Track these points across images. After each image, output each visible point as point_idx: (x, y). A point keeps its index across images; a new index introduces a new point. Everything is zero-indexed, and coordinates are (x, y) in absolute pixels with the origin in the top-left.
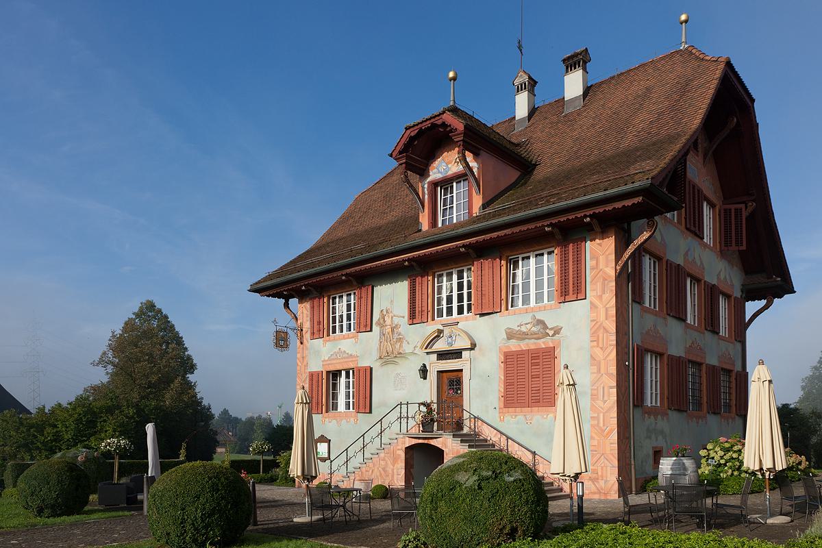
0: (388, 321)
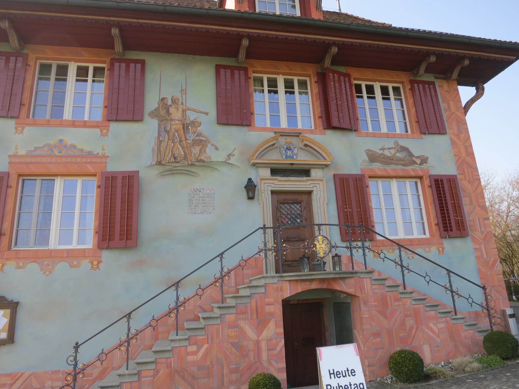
0: (176, 114)
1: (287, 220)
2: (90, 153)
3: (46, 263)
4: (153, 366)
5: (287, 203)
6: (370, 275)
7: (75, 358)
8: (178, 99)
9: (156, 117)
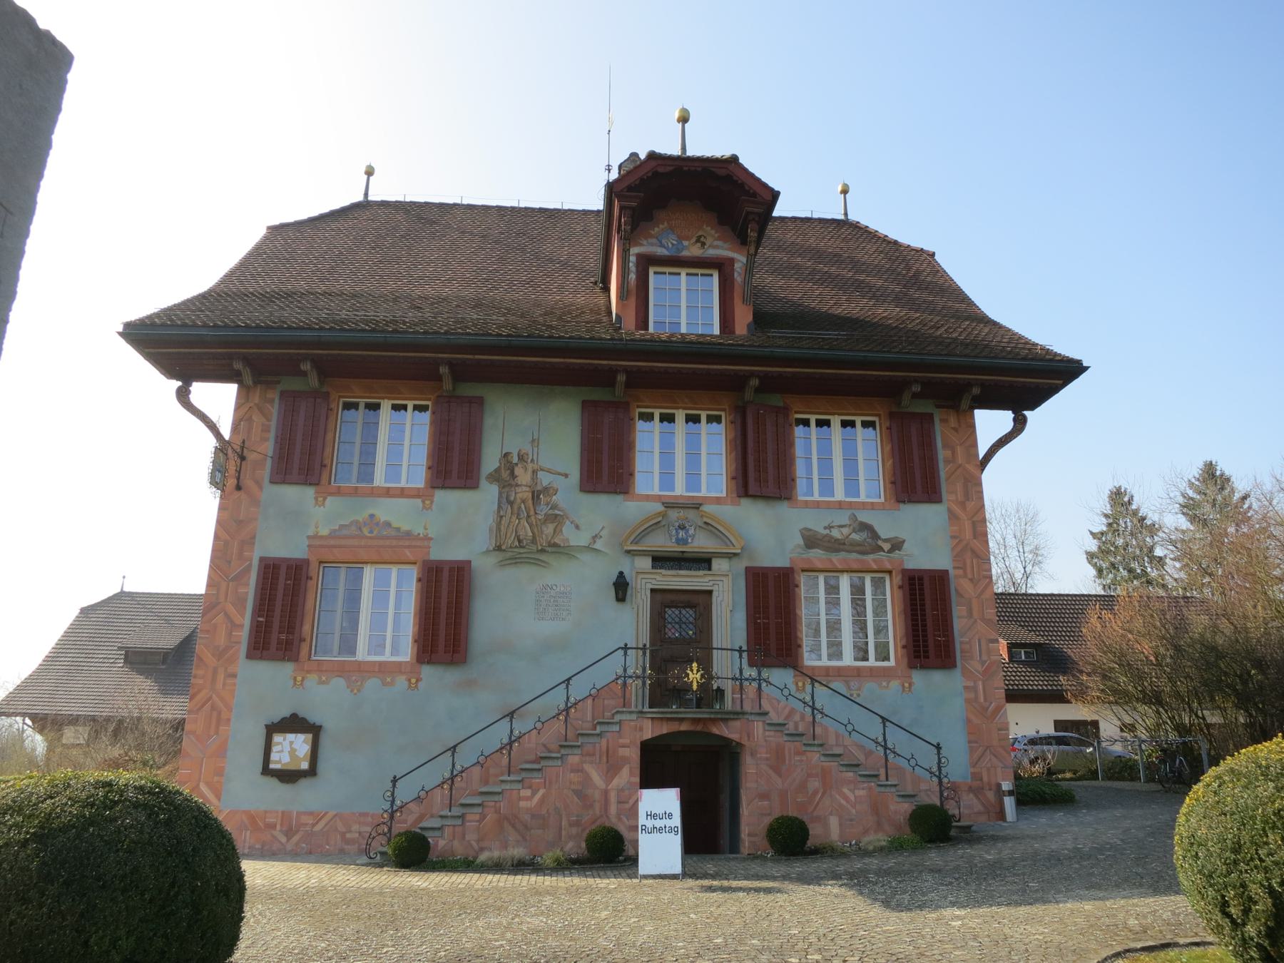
0: (523, 477)
1: (673, 631)
2: (408, 533)
3: (354, 678)
4: (479, 810)
5: (676, 607)
6: (762, 718)
7: (393, 794)
8: (527, 455)
9: (495, 480)
